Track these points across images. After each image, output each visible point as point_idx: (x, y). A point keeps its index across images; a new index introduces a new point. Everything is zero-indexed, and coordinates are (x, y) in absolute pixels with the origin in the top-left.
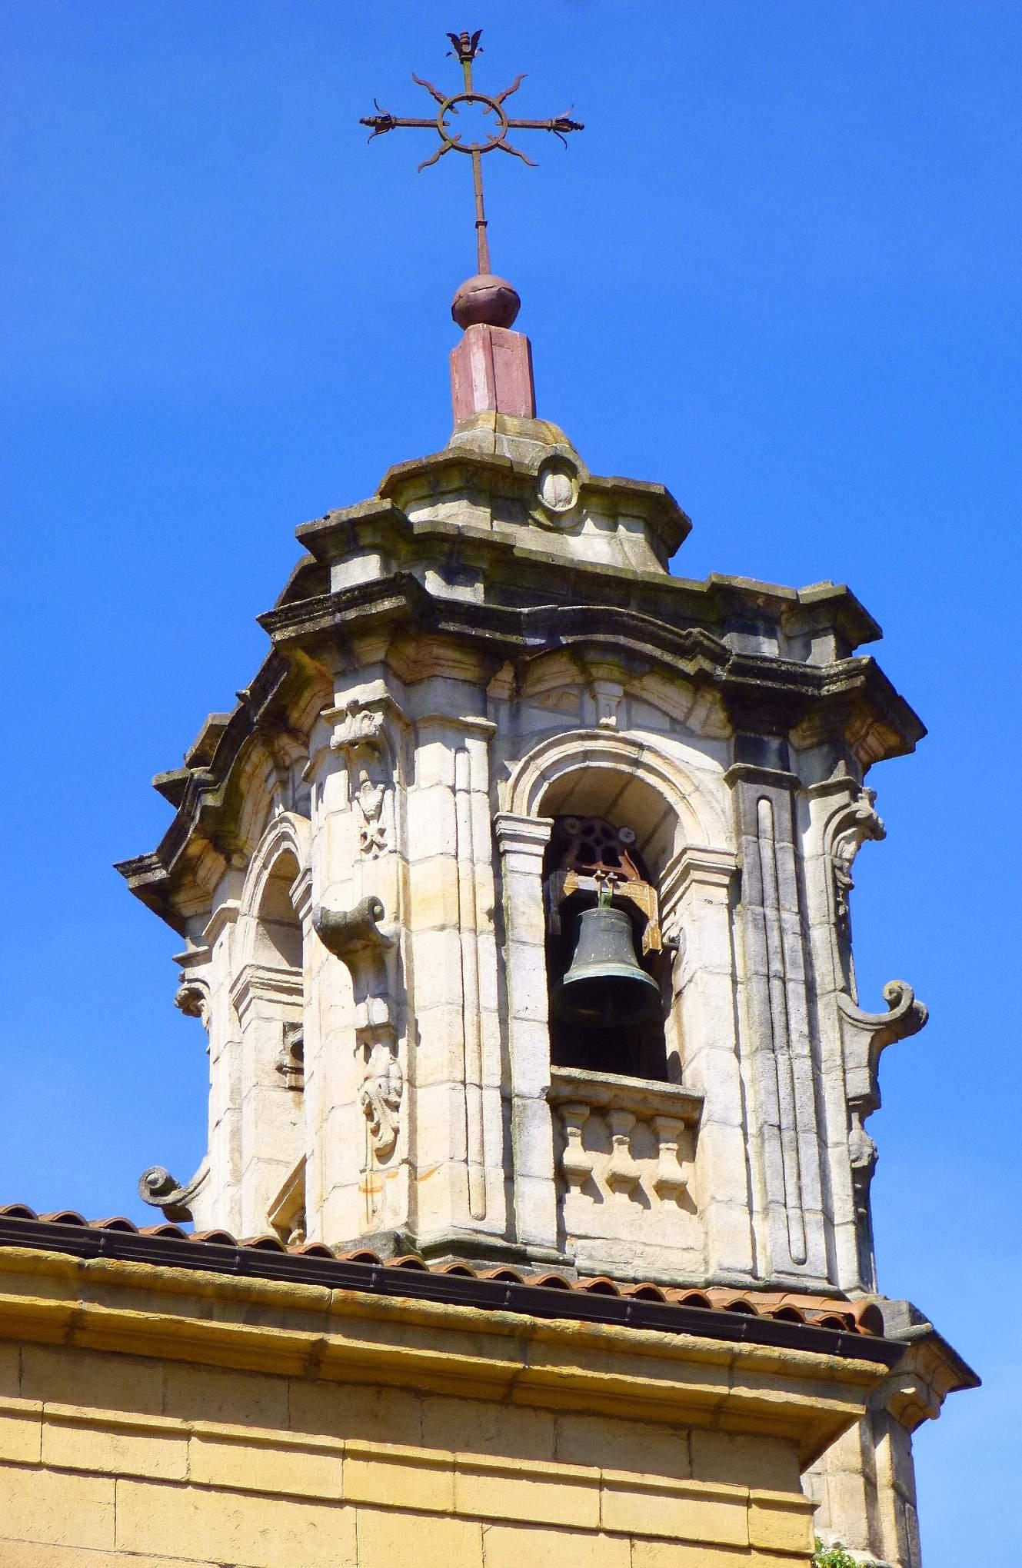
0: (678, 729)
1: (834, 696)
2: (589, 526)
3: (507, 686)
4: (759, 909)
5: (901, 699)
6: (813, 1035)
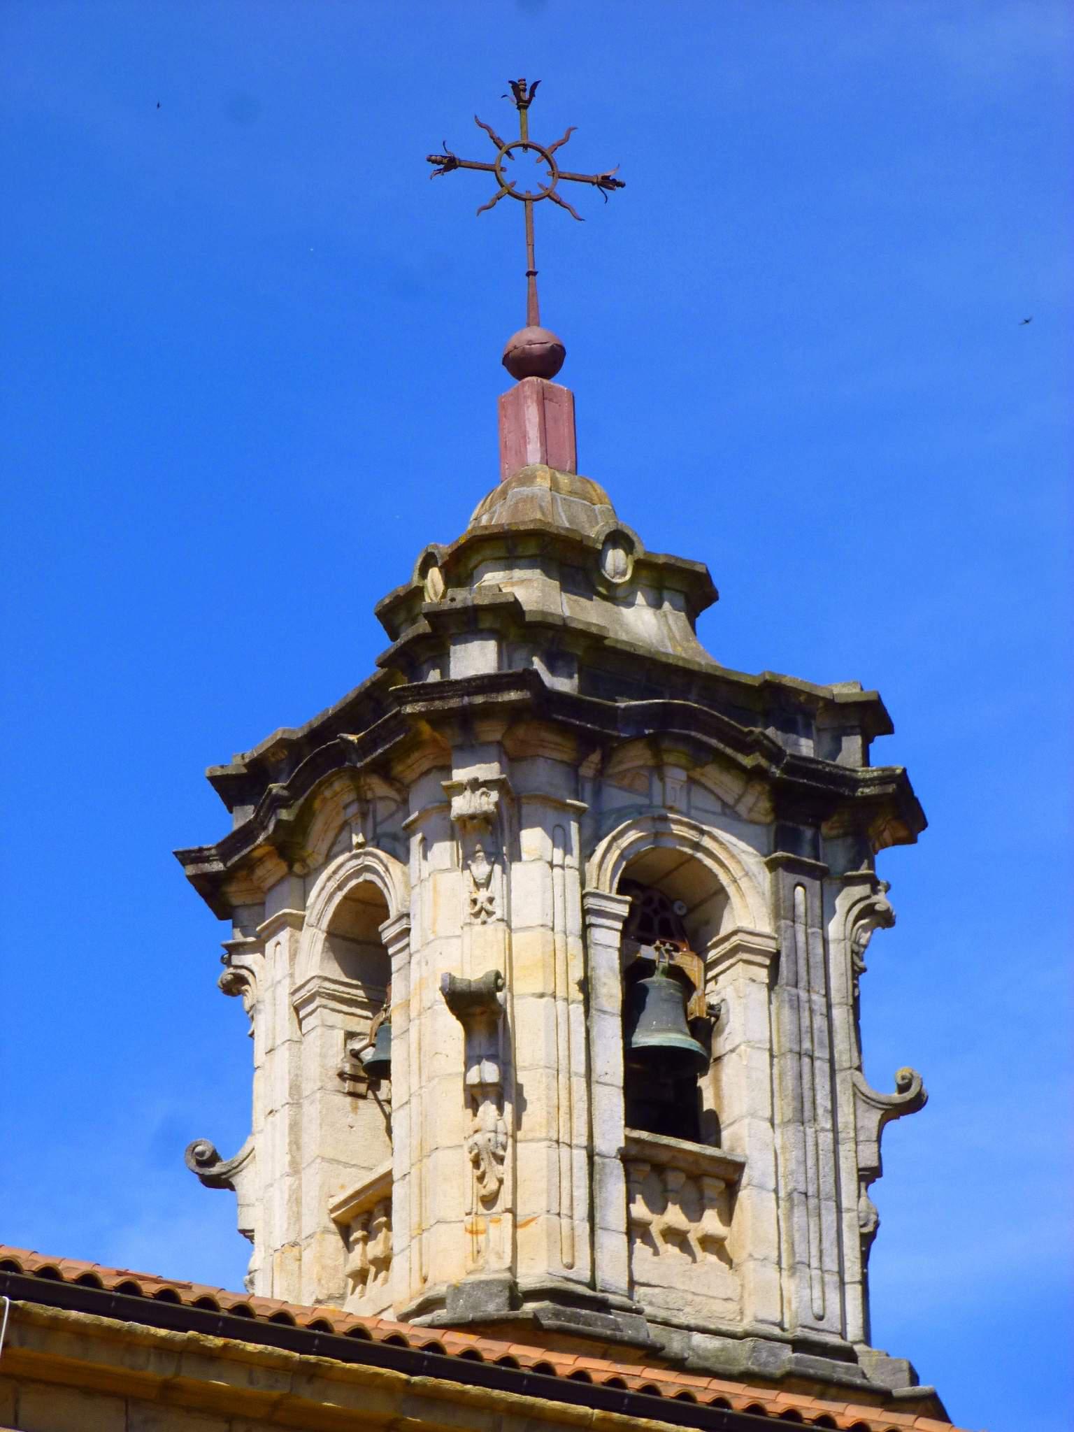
0: (730, 815)
1: (866, 798)
2: (640, 599)
3: (593, 766)
4: (794, 991)
5: (916, 800)
6: (834, 1112)
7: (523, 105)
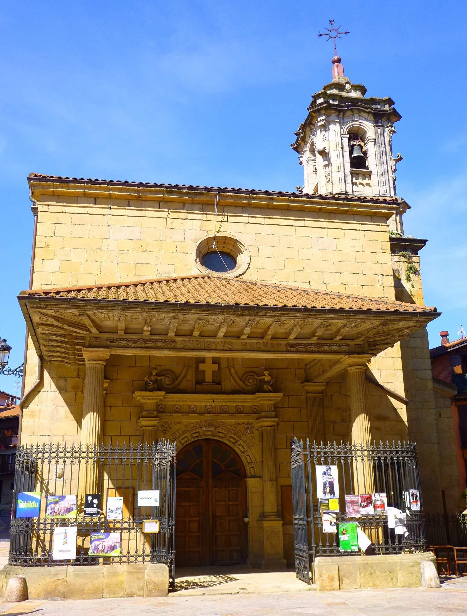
0: (366, 120)
7: (332, 24)
